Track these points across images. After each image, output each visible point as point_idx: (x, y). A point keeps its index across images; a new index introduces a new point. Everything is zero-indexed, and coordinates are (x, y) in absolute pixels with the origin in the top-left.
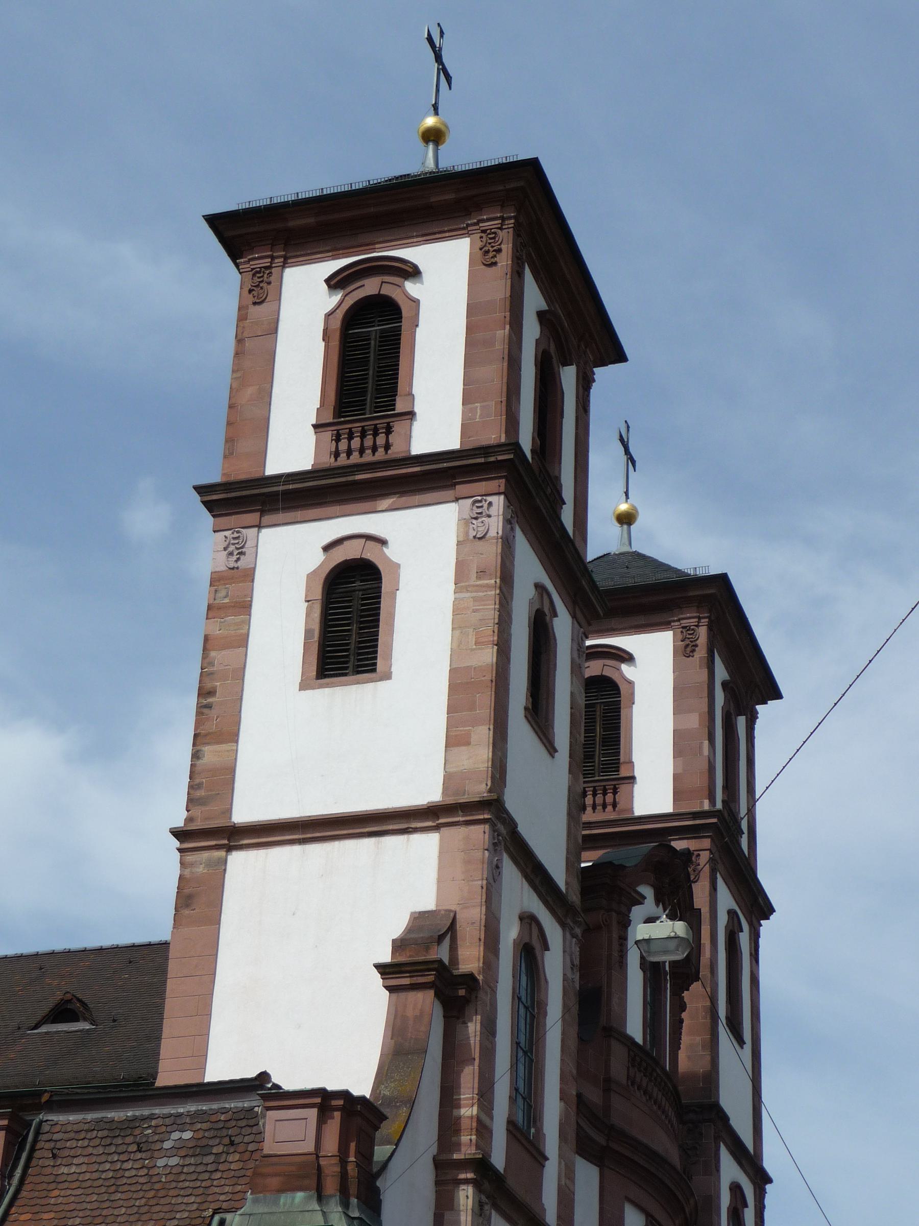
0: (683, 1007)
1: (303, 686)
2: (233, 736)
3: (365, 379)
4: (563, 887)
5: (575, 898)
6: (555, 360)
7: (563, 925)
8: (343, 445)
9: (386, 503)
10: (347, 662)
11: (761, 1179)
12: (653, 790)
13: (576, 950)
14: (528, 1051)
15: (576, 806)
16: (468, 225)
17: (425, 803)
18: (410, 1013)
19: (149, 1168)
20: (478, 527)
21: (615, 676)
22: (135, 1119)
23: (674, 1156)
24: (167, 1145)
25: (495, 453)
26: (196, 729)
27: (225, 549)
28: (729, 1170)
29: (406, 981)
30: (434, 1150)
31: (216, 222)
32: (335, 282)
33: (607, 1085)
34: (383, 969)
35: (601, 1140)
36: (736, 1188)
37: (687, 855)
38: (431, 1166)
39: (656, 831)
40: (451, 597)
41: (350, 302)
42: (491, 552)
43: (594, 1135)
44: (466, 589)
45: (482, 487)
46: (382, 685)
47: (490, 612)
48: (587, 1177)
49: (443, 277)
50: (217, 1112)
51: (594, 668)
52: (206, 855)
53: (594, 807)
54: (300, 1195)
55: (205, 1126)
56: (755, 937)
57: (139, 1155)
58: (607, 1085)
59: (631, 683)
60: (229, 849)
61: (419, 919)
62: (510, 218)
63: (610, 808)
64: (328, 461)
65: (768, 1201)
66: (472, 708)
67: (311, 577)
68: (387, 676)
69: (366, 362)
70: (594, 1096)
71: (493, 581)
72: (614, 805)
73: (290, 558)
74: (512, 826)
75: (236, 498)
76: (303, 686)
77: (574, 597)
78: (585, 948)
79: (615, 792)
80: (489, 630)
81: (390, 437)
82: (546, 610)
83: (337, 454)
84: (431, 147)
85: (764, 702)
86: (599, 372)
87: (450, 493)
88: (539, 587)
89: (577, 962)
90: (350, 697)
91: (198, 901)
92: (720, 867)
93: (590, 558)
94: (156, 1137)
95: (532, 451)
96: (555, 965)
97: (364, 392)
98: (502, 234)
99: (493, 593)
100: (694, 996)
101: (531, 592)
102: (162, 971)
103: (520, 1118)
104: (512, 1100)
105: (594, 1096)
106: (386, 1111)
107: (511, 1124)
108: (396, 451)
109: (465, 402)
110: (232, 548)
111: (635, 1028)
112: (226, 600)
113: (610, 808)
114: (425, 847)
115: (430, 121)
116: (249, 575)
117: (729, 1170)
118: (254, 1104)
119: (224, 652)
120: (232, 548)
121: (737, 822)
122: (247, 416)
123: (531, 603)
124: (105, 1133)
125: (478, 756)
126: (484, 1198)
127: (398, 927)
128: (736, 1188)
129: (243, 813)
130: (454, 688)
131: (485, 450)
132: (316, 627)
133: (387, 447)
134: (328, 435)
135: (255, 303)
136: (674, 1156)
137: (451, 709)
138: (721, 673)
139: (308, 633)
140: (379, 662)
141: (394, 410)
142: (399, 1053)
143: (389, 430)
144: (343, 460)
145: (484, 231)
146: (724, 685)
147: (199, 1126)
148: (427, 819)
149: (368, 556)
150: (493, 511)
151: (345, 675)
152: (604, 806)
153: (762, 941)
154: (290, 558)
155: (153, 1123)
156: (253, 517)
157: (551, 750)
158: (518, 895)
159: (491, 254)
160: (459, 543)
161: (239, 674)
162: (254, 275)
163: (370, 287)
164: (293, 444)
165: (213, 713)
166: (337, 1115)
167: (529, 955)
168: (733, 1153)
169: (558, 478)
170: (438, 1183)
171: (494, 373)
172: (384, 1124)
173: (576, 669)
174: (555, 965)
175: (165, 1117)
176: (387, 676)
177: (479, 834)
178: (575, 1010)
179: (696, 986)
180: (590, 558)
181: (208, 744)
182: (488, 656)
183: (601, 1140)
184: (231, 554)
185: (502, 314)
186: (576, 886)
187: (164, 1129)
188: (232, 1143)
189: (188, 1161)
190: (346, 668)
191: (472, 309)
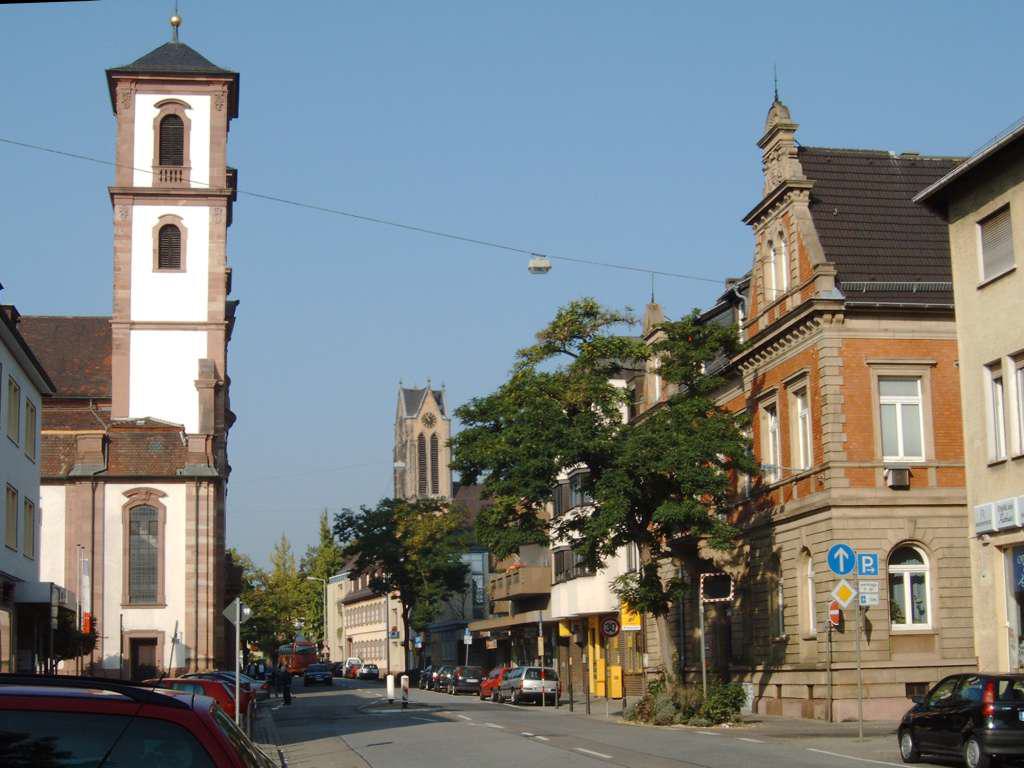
2: (127, 286)
8: (164, 177)
32: (160, 105)
34: (196, 381)
40: (208, 245)
41: (164, 115)
49: (200, 109)
53: (176, 180)
59: (190, 121)
60: (131, 329)
67: (155, 120)
68: (184, 271)
73: (146, 219)
81: (462, 487)
90: (169, 277)
109: (211, 166)
114: (202, 337)
115: (174, 19)
122: (125, 163)
129: (134, 318)
131: (221, 190)
139: (154, 251)
140: (182, 265)
152: (176, 180)
154: (146, 219)
161: (129, 263)
164: (144, 175)
176: (184, 271)
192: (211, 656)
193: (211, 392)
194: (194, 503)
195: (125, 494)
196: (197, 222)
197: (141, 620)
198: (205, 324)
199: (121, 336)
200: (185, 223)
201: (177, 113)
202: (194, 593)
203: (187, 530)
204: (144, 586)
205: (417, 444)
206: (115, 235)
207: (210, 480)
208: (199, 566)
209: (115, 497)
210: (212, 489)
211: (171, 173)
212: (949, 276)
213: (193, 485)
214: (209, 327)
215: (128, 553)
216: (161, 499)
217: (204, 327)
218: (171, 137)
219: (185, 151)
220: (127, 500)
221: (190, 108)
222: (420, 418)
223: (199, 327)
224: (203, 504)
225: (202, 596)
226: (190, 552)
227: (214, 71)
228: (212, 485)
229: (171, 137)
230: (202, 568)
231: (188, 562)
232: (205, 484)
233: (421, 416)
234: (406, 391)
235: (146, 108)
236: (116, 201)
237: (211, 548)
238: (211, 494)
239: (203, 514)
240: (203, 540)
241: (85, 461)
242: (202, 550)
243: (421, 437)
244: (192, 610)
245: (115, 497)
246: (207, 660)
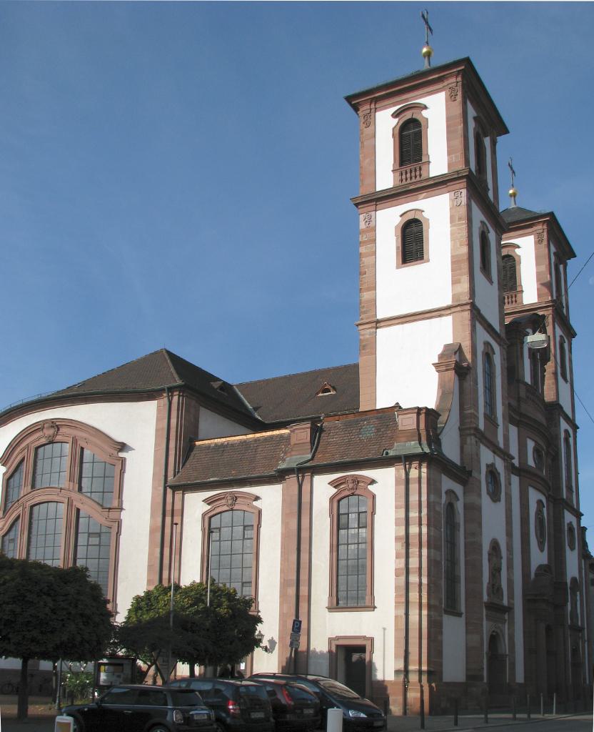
0: (545, 371)
1: (398, 268)
4: (499, 332)
5: (503, 335)
6: (482, 136)
7: (500, 345)
8: (404, 177)
11: (575, 427)
12: (530, 293)
13: (505, 353)
14: (490, 389)
15: (502, 303)
21: (513, 254)
23: (544, 421)
28: (564, 425)
30: (458, 424)
31: (349, 99)
32: (395, 115)
33: (519, 400)
35: (518, 418)
36: (566, 431)
37: (543, 316)
38: (458, 431)
39: (532, 309)
40: (449, 229)
41: (401, 122)
42: (463, 211)
43: (516, 417)
44: (454, 226)
45: (458, 186)
47: (465, 233)
48: (513, 430)
49: (436, 109)
51: (504, 252)
52: (368, 331)
56: (570, 344)
58: (519, 400)
59: (519, 256)
60: (377, 328)
61: (447, 347)
63: (514, 303)
64: (398, 183)
65: (578, 435)
66: (460, 269)
67: (396, 227)
68: (428, 261)
70: (514, 403)
71: (464, 222)
72: (516, 301)
73: (388, 221)
74: (478, 311)
76: (398, 268)
77: (490, 222)
78: (508, 353)
79: (516, 297)
80: (465, 240)
82: (486, 230)
85: (569, 259)
86: (499, 138)
88: (482, 222)
89: (505, 357)
90: (414, 270)
92: (556, 320)
93: (500, 211)
95: (476, 171)
96: (497, 359)
99: (465, 226)
100: (550, 367)
101: (479, 225)
102: (357, 373)
103: (488, 412)
104: (485, 407)
105: (514, 403)
106: (441, 414)
107: (485, 414)
108: (424, 176)
111: (528, 379)
113: (514, 303)
114: (447, 321)
116: (374, 229)
117: (564, 425)
121: (561, 303)
123: (480, 228)
125: (465, 286)
126: (477, 440)
127: (440, 350)
128: (566, 431)
129: (379, 317)
130: (453, 263)
131: (457, 172)
132: (400, 245)
133: (420, 176)
136: (544, 421)
137: (452, 270)
138: (553, 249)
139: (397, 248)
142: (444, 394)
143: (420, 169)
144: (404, 182)
146: (554, 253)
152: (512, 302)
153: (572, 346)
154: (388, 221)
157: (491, 282)
158: (483, 336)
160: (450, 209)
164: (385, 178)
167: (488, 357)
168: (564, 419)
169: (486, 180)
170: (461, 436)
171: (459, 143)
172: (440, 417)
173: (499, 252)
174: (497, 359)
176: (428, 261)
177: (467, 315)
178: (505, 374)
179: (549, 363)
180: (500, 211)
182: (465, 250)
183: (518, 418)
185: (460, 120)
186: (504, 331)
191: (448, 119)
192: (424, 668)
193: (451, 374)
194: (403, 487)
195: (206, 501)
197: (349, 625)
198: (449, 308)
199: (367, 336)
201: (510, 254)
202: (404, 592)
204: (352, 590)
206: (360, 243)
207: (421, 458)
208: (410, 560)
209: (323, 487)
210: (424, 470)
211: (411, 172)
212: (442, 659)
213: (401, 467)
214: (453, 310)
216: (370, 487)
217: (449, 312)
218: (410, 142)
220: (334, 491)
221: (519, 247)
223: (442, 312)
224: (414, 487)
225: (414, 596)
226: (400, 544)
227: (529, 216)
228: (424, 465)
229: (410, 142)
230: (414, 562)
231: (397, 557)
232: (415, 464)
235: (385, 122)
237: (425, 538)
238: (424, 475)
239: (414, 498)
240: (414, 530)
242: (414, 540)
244: (402, 612)
245: (323, 487)
246: (420, 672)
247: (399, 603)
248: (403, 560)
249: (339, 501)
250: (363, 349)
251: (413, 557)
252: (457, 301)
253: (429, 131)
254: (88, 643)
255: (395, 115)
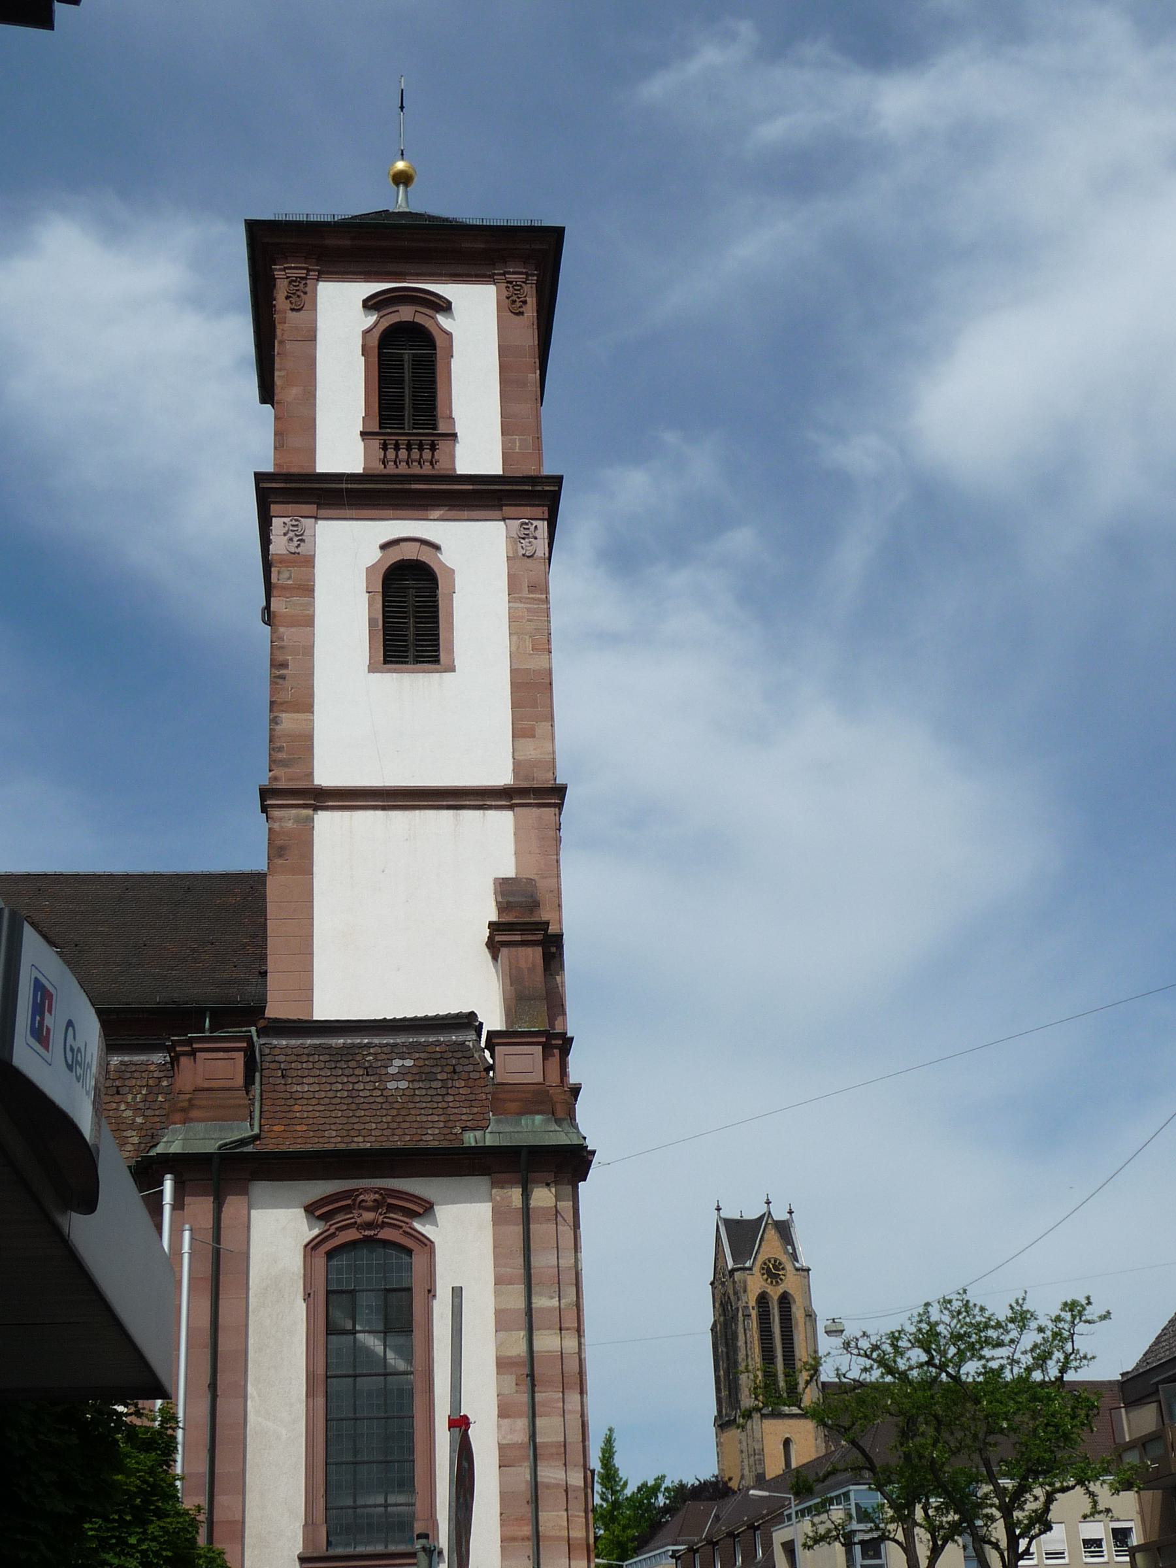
1: (372, 669)
2: (306, 705)
3: (401, 396)
9: (436, 514)
10: (406, 652)
16: (495, 274)
17: (502, 784)
18: (523, 965)
19: (382, 1090)
20: (527, 547)
22: (353, 1046)
24: (391, 1070)
25: (543, 484)
26: (271, 696)
27: (285, 534)
29: (518, 938)
32: (370, 304)
40: (507, 606)
41: (385, 324)
44: (520, 600)
45: (528, 511)
46: (447, 676)
50: (432, 1043)
52: (294, 811)
54: (538, 1118)
55: (423, 1055)
57: (368, 1079)
60: (316, 808)
62: (533, 275)
67: (370, 570)
68: (452, 669)
69: (401, 381)
73: (347, 555)
75: (295, 489)
76: (372, 669)
83: (384, 462)
84: (401, 188)
87: (498, 514)
90: (410, 686)
91: (293, 853)
94: (379, 1064)
97: (402, 409)
98: (526, 288)
108: (442, 467)
109: (505, 431)
110: (291, 534)
112: (290, 582)
115: (400, 165)
118: (469, 1038)
119: (293, 630)
120: (291, 534)
124: (327, 1058)
129: (325, 776)
130: (515, 686)
134: (376, 443)
135: (292, 310)
137: (514, 706)
139: (372, 622)
141: (435, 429)
143: (433, 448)
144: (391, 469)
145: (511, 282)
147: (417, 1055)
148: (500, 799)
149: (423, 558)
150: (539, 534)
151: (406, 663)
154: (347, 555)
155: (372, 1051)
156: (311, 509)
159: (518, 304)
161: (308, 651)
162: (290, 283)
163: (406, 313)
165: (288, 683)
166: (556, 1052)
175: (381, 1046)
181: (285, 712)
184: (291, 540)
187: (384, 1057)
188: (454, 1072)
189: (417, 1085)
190: (407, 657)
196: (473, 555)
199: (290, 824)
200: (448, 557)
203: (498, 1313)
205: (754, 1313)
208: (539, 1422)
209: (278, 1235)
215: (321, 1389)
219: (440, 395)
222: (756, 1269)
225: (553, 1519)
226: (510, 1380)
233: (759, 1263)
234: (728, 1223)
236: (274, 509)
241: (194, 1113)
243: (763, 1299)
247: (514, 1539)
248: (522, 1423)
249: (330, 1255)
250: (280, 856)
251: (548, 1415)
252: (526, 779)
253: (456, 364)
254: (812, 1377)
255: (370, 304)
